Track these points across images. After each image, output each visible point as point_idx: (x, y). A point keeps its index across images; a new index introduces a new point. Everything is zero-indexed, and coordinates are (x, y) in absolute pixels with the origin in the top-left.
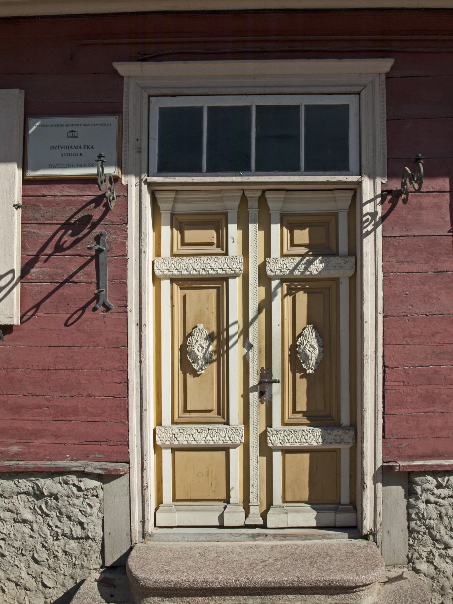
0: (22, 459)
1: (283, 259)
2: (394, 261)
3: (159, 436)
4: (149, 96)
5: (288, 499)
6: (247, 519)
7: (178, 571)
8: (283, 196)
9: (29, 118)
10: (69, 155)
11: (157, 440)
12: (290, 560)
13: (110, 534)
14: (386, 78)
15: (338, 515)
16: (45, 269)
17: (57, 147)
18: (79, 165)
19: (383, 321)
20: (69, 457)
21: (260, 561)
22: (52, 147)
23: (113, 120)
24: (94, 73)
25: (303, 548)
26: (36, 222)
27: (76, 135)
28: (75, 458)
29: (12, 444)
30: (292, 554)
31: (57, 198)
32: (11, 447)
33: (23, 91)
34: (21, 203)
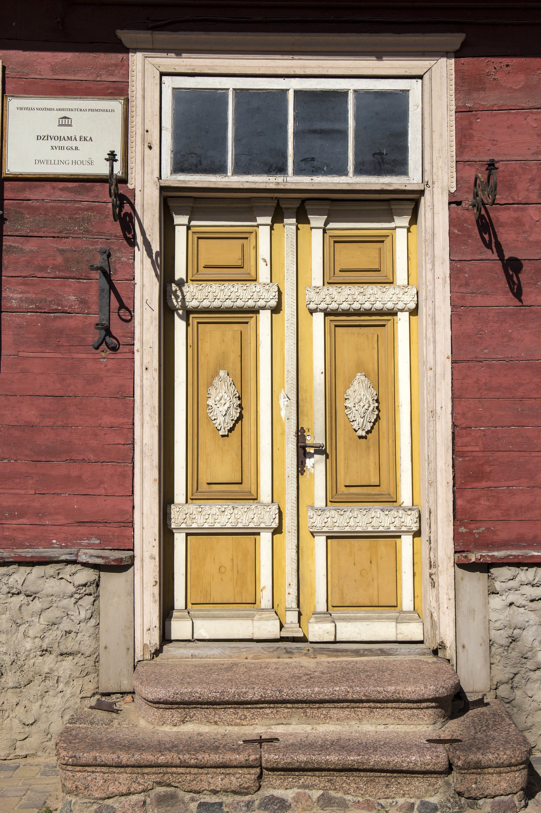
4: (162, 74)
6: (283, 629)
8: (328, 207)
9: (8, 98)
10: (62, 148)
15: (400, 626)
16: (29, 295)
17: (46, 138)
18: (74, 161)
20: (56, 543)
22: (38, 138)
23: (117, 105)
26: (17, 233)
28: (63, 544)
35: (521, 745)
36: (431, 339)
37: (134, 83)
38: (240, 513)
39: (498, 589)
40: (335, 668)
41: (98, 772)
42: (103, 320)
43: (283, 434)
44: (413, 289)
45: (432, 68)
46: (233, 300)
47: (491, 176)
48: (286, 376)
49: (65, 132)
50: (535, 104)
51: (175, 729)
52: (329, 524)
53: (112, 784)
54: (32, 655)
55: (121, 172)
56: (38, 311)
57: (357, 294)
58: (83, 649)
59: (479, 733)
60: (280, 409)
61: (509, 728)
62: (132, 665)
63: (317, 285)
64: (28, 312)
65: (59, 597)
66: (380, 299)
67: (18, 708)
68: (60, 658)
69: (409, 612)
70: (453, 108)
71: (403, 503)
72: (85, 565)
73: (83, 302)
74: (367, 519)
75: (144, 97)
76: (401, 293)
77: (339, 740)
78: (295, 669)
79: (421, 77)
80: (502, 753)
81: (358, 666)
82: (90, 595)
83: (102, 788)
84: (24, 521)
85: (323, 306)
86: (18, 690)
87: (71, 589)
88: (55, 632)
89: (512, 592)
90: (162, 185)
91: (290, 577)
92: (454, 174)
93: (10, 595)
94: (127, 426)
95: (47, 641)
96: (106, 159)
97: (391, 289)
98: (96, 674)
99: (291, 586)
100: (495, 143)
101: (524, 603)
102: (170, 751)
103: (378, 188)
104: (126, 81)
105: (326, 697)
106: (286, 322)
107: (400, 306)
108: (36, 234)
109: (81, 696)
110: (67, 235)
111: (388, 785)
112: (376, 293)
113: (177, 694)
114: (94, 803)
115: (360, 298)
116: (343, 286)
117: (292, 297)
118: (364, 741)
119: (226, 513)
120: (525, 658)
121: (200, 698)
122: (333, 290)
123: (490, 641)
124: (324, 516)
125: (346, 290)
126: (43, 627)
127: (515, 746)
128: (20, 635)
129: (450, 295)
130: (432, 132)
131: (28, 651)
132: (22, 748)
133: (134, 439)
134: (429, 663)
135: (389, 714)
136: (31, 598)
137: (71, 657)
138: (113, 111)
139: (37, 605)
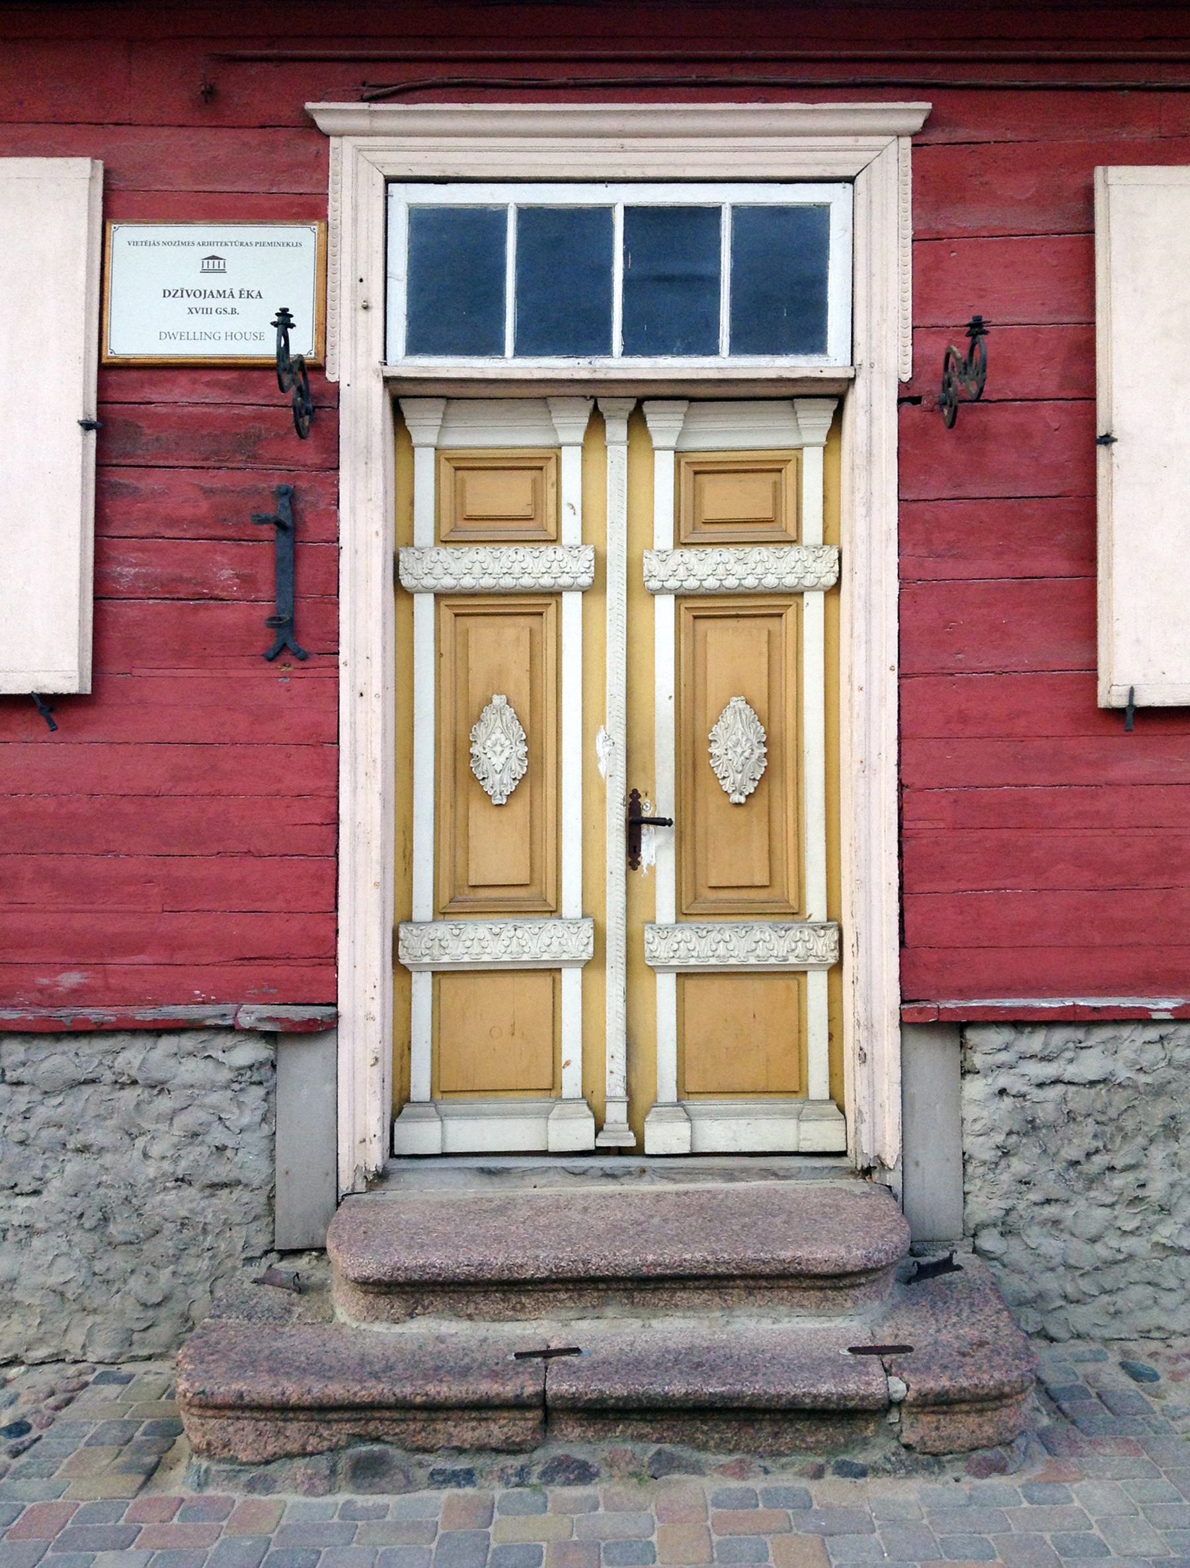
0: (89, 1004)
1: (678, 551)
2: (926, 555)
3: (406, 944)
4: (389, 180)
5: (690, 1087)
6: (600, 1135)
7: (446, 1244)
11: (400, 953)
12: (697, 1221)
13: (287, 1173)
14: (913, 146)
15: (805, 1126)
16: (151, 570)
17: (179, 294)
19: (899, 687)
21: (630, 1222)
22: (166, 293)
23: (305, 235)
24: (262, 127)
25: (727, 1196)
27: (222, 267)
28: (213, 998)
29: (67, 967)
30: (702, 1208)
31: (179, 410)
32: (63, 975)
33: (100, 163)
34: (94, 418)
35: (1020, 1359)
36: (863, 638)
37: (338, 196)
38: (526, 936)
39: (977, 1066)
40: (689, 1206)
41: (246, 1418)
42: (283, 611)
43: (603, 800)
44: (832, 552)
45: (872, 164)
46: (517, 576)
47: (977, 346)
48: (608, 704)
49: (214, 282)
50: (1053, 227)
51: (397, 1329)
52: (682, 953)
53: (273, 1439)
54: (159, 1187)
55: (313, 352)
56: (167, 596)
57: (732, 561)
58: (245, 1176)
59: (944, 1331)
60: (597, 759)
61: (998, 1318)
62: (335, 1201)
63: (662, 548)
64: (149, 598)
65: (204, 1089)
66: (773, 571)
67: (134, 1278)
68: (208, 1192)
69: (822, 1101)
70: (910, 233)
71: (810, 916)
72: (251, 1033)
73: (247, 581)
74: (747, 944)
75: (355, 221)
76: (811, 558)
77: (690, 1350)
78: (617, 1212)
79: (851, 180)
80: (986, 1377)
81: (729, 1202)
82: (261, 1083)
83: (256, 1446)
84: (142, 958)
85: (672, 583)
86: (133, 1248)
87: (225, 1075)
88: (199, 1149)
89: (1004, 1070)
90: (387, 375)
91: (615, 1045)
92: (910, 348)
93: (118, 1086)
94: (327, 793)
95: (183, 1164)
96: (272, 324)
97: (792, 553)
98: (270, 1219)
99: (616, 1060)
100: (982, 293)
101: (1024, 1089)
102: (378, 1379)
103: (772, 374)
104: (320, 191)
105: (668, 1271)
106: (608, 612)
107: (809, 581)
108: (161, 463)
109: (244, 1256)
110: (217, 464)
111: (778, 1433)
112: (766, 559)
113: (399, 1269)
114: (240, 1471)
115: (740, 570)
116: (709, 550)
117: (619, 568)
118: (736, 1353)
119: (502, 937)
120: (1026, 1183)
121: (439, 1275)
122: (690, 555)
123: (964, 1154)
124: (671, 940)
125: (714, 555)
126: (175, 1140)
127: (1010, 1360)
128: (137, 1154)
129: (897, 560)
130: (870, 275)
131: (150, 1181)
132: (143, 1343)
133: (338, 814)
134: (856, 1196)
135: (782, 1299)
136: (155, 1092)
137: (227, 1190)
138: (299, 245)
139: (164, 1104)
